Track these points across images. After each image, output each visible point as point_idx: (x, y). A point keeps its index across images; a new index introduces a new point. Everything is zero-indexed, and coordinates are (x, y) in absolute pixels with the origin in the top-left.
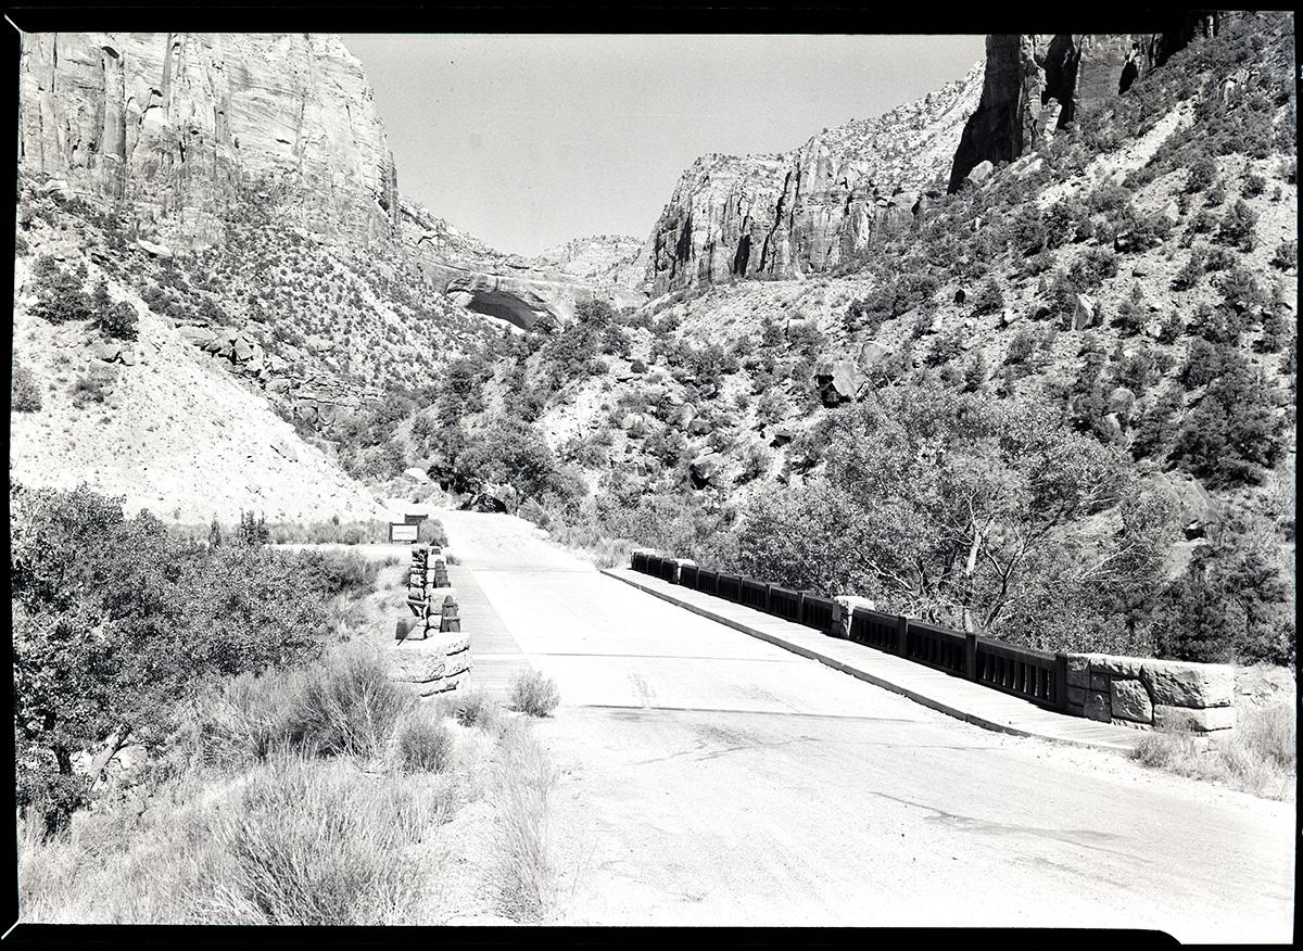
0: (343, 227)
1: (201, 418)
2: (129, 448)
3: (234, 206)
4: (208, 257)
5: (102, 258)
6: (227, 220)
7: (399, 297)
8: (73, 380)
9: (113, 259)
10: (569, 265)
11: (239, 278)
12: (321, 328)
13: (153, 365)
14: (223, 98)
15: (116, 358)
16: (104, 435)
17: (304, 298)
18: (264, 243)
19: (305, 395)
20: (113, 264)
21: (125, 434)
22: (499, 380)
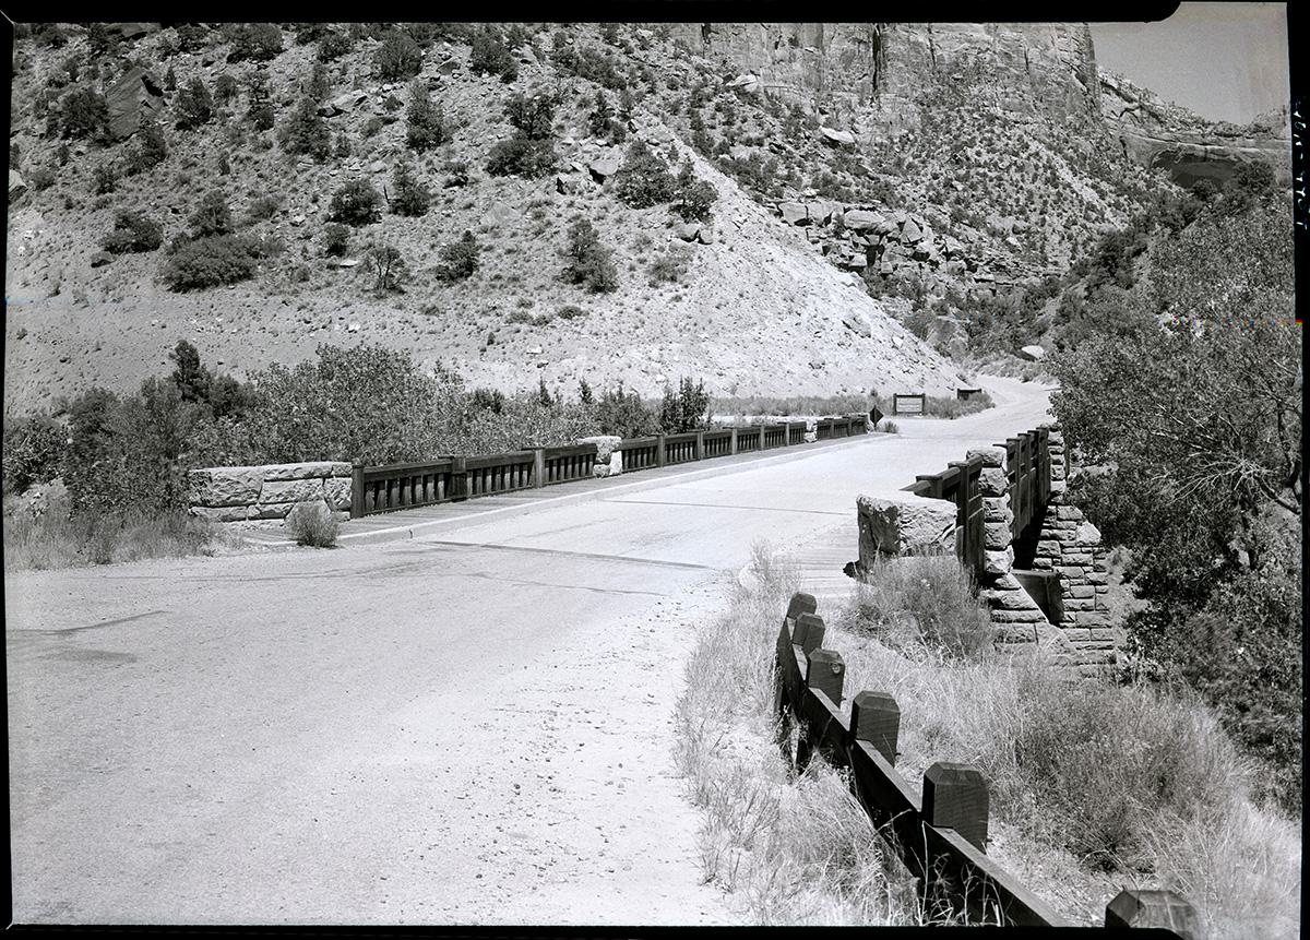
0: (1038, 104)
1: (773, 294)
2: (695, 325)
3: (929, 90)
4: (904, 140)
5: (778, 146)
6: (923, 105)
7: (1098, 172)
8: (652, 261)
9: (789, 147)
11: (934, 162)
12: (1016, 209)
13: (729, 242)
15: (695, 237)
19: (983, 277)
20: (789, 152)
21: (694, 312)
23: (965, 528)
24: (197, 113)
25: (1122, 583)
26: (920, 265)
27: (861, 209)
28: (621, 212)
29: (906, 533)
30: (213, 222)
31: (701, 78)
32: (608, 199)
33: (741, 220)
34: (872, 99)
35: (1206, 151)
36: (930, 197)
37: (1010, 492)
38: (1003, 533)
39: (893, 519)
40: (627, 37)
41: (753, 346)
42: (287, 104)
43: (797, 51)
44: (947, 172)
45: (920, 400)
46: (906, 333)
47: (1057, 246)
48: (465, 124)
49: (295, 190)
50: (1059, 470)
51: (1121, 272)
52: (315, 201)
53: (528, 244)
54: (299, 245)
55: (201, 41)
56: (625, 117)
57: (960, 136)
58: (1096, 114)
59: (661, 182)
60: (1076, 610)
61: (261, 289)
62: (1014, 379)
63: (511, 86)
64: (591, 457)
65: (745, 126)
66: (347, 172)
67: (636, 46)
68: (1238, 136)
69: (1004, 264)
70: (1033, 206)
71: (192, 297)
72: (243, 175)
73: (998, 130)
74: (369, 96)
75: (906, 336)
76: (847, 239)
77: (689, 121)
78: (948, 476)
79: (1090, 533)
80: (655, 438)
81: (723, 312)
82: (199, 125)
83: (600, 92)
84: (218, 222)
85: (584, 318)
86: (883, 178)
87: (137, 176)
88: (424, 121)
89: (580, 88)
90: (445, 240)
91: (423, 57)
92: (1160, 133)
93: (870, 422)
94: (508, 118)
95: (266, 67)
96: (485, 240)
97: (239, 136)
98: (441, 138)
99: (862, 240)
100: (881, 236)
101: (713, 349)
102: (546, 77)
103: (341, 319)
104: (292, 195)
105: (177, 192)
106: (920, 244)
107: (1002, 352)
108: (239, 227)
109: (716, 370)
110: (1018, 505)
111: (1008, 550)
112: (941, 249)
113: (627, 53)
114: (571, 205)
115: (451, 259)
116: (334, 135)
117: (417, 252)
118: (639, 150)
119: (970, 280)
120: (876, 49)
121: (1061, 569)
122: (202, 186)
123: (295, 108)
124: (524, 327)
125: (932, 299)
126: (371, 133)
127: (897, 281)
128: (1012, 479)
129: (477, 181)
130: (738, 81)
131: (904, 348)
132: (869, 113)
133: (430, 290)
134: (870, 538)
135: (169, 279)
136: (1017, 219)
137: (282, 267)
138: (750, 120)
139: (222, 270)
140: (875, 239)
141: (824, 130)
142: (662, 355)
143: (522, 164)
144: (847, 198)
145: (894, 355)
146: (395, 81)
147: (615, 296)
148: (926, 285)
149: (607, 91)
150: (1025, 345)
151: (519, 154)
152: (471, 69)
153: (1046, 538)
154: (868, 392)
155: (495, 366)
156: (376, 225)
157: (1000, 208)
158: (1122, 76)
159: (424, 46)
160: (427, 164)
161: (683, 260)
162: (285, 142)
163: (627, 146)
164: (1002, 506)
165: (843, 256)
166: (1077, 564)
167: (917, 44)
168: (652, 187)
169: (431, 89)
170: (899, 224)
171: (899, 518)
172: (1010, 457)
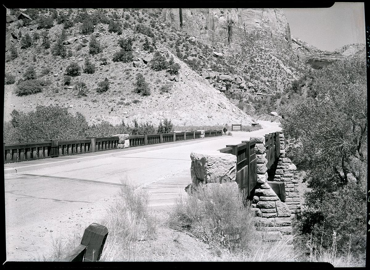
0: (274, 46)
4: (237, 56)
5: (201, 57)
7: (291, 65)
8: (161, 86)
9: (204, 57)
10: (343, 53)
11: (245, 62)
13: (184, 81)
14: (240, 12)
16: (167, 102)
17: (264, 67)
18: (252, 52)
19: (259, 94)
20: (204, 58)
21: (173, 101)
22: (307, 86)
23: (248, 166)
24: (27, 44)
25: (302, 183)
26: (241, 90)
27: (224, 74)
28: (152, 72)
29: (209, 171)
30: (30, 76)
31: (179, 37)
32: (148, 68)
33: (187, 74)
34: (228, 44)
35: (321, 59)
36: (244, 71)
37: (267, 153)
38: (264, 168)
39: (204, 164)
40: (158, 26)
41: (191, 111)
42: (54, 41)
43: (207, 31)
44: (249, 65)
45: (240, 126)
46: (237, 108)
47: (280, 85)
48: (107, 47)
49: (56, 66)
50: (282, 146)
51: (298, 91)
52: (61, 69)
53: (124, 82)
54: (56, 82)
55: (30, 23)
56: (154, 45)
57: (252, 54)
58: (290, 49)
59: (164, 63)
60: (288, 192)
61: (44, 95)
62: (269, 121)
63: (120, 36)
64: (117, 141)
65: (192, 51)
66: (71, 61)
67: (161, 28)
68: (330, 55)
69: (265, 90)
70: (273, 74)
71: (24, 97)
72: (40, 62)
73: (263, 53)
74: (78, 39)
75: (236, 109)
76: (220, 83)
77: (175, 49)
78: (241, 146)
79: (293, 167)
80: (143, 135)
81: (182, 101)
82: (28, 47)
83: (146, 38)
84: (32, 75)
85: (140, 103)
86: (231, 66)
87: (9, 62)
88: (94, 46)
89: (140, 37)
90: (99, 81)
91: (95, 28)
92: (308, 54)
93: (223, 132)
94: (119, 45)
95: (48, 30)
96: (112, 81)
97: (39, 50)
98: (99, 51)
99: (225, 83)
100: (230, 82)
101: (179, 112)
102: (131, 34)
103: (67, 104)
104: (55, 68)
105: (20, 67)
106: (241, 84)
107: (265, 114)
108: (38, 77)
109: (180, 118)
110: (269, 157)
111: (266, 174)
112: (247, 86)
113: (158, 30)
114: (137, 70)
115: (101, 86)
116: (68, 50)
117: (91, 84)
118: (158, 54)
119: (255, 94)
120: (229, 30)
121: (283, 178)
122: (28, 65)
123: (56, 42)
124: (122, 106)
125: (245, 100)
126: (78, 50)
127: (235, 95)
128: (267, 148)
129: (109, 63)
130: (190, 38)
131: (236, 112)
132: (227, 48)
133: (94, 95)
134: (194, 173)
135: (17, 92)
136: (269, 78)
137: (51, 89)
138: (193, 49)
139: (32, 90)
140: (228, 83)
141: (214, 52)
142: (163, 114)
143: (123, 58)
144: (220, 71)
145: (233, 114)
146: (86, 34)
147: (150, 97)
148: (243, 96)
149: (149, 37)
150: (271, 112)
151: (123, 55)
152: (109, 31)
153: (279, 168)
154: (225, 124)
155: (113, 118)
156: (79, 76)
157: (264, 75)
158: (298, 38)
159: (95, 24)
160: (95, 59)
161: (170, 86)
162: (53, 52)
163: (154, 53)
164: (263, 158)
165: (219, 87)
166: (288, 177)
167: (240, 29)
168: (161, 65)
169: (96, 37)
170: (235, 78)
171: (206, 163)
172: (266, 141)
